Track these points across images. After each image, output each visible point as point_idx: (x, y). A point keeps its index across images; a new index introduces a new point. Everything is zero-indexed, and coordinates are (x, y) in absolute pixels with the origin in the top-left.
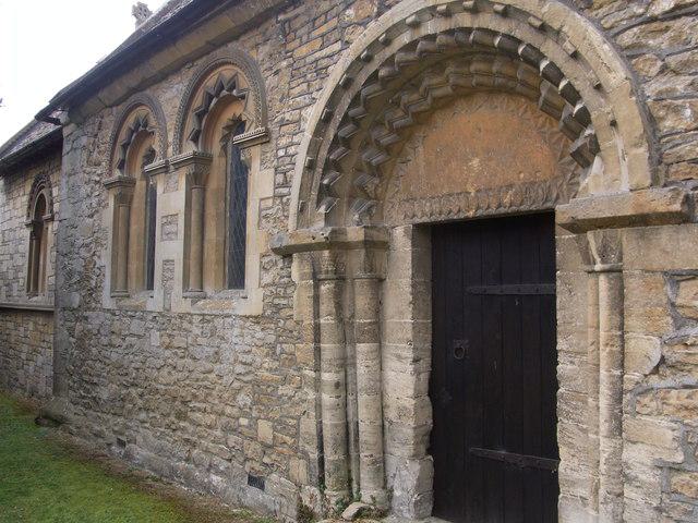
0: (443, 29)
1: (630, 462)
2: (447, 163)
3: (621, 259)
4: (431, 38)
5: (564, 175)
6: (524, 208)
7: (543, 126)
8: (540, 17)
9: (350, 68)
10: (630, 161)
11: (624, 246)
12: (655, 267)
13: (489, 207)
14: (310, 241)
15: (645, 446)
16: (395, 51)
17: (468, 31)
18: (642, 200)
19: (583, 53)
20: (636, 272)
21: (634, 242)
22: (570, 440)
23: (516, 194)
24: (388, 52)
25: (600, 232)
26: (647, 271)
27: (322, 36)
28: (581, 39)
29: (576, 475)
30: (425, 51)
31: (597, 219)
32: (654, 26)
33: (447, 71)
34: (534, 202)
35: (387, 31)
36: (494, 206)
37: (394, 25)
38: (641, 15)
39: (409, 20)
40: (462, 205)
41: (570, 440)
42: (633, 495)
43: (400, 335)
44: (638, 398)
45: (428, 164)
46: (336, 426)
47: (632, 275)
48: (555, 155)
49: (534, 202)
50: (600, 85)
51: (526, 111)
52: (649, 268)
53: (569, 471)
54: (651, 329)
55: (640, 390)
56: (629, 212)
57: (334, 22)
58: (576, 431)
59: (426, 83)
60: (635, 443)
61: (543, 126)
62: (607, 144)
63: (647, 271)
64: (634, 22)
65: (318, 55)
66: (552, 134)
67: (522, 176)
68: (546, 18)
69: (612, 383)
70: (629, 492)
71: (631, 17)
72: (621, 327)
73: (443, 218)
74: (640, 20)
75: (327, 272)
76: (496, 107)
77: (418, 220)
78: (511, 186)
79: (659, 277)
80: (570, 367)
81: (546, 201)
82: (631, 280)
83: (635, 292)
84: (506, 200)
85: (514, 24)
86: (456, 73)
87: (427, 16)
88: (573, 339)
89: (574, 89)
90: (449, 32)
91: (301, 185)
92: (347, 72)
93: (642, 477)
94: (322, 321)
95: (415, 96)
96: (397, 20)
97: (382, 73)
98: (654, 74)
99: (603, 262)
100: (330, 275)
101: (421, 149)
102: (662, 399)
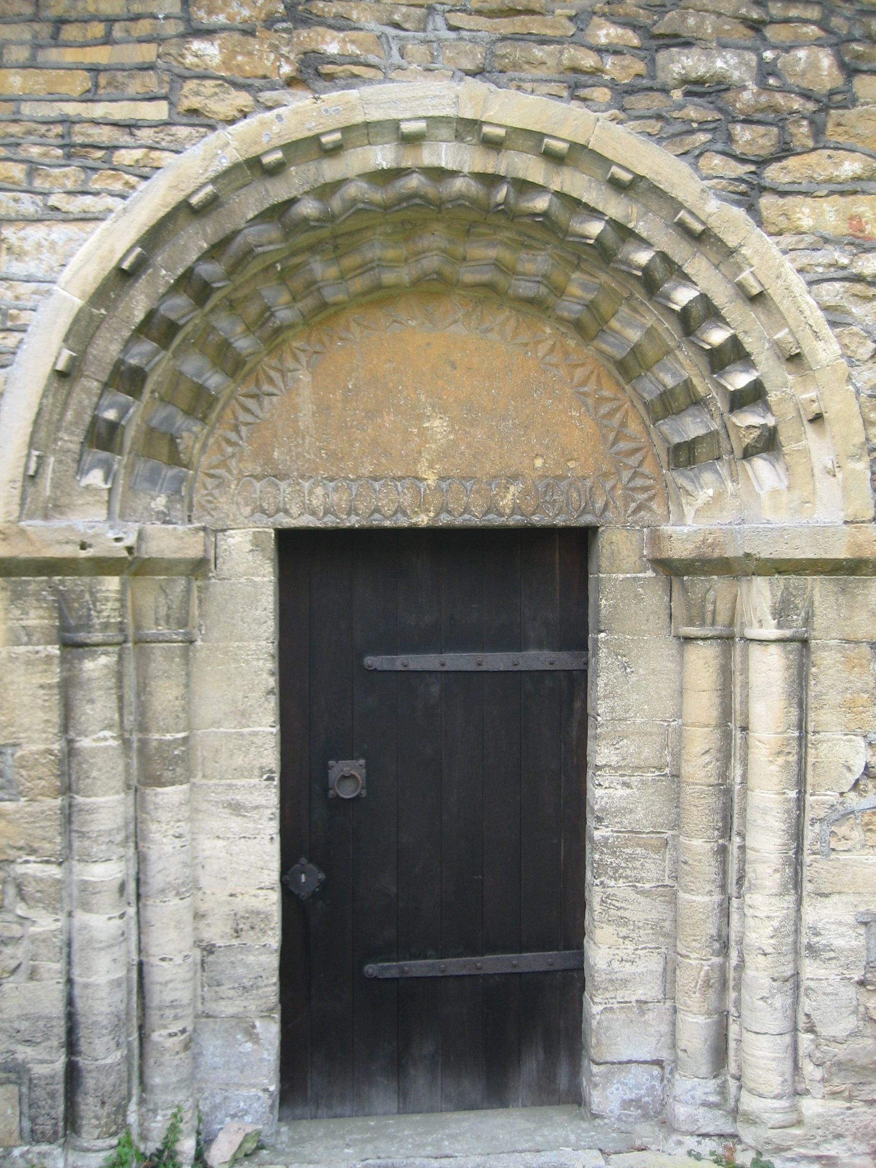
0: (478, 169)
1: (820, 925)
2: (372, 414)
3: (808, 621)
4: (439, 174)
5: (618, 473)
6: (537, 520)
7: (584, 383)
8: (703, 218)
9: (226, 173)
10: (845, 479)
11: (816, 604)
12: (860, 636)
13: (466, 510)
14: (71, 551)
15: (844, 898)
16: (351, 173)
17: (524, 187)
18: (861, 538)
19: (777, 299)
20: (833, 642)
21: (832, 598)
22: (619, 913)
23: (526, 492)
24: (331, 170)
25: (781, 580)
26: (848, 641)
27: (94, 70)
28: (773, 276)
29: (628, 968)
30: (421, 197)
31: (790, 560)
32: (859, 288)
33: (425, 242)
34: (560, 511)
35: (346, 130)
36: (477, 511)
37: (367, 124)
38: (844, 268)
39: (407, 127)
40: (407, 500)
41: (619, 913)
42: (822, 973)
43: (239, 760)
44: (833, 828)
45: (323, 409)
46: (117, 983)
47: (825, 647)
48: (604, 437)
49: (560, 511)
50: (798, 355)
51: (552, 350)
52: (852, 637)
53: (616, 965)
54: (853, 726)
55: (835, 816)
56: (841, 553)
57: (147, 53)
58: (633, 895)
59: (375, 252)
60: (826, 895)
61: (584, 383)
62: (794, 446)
63: (848, 641)
64: (832, 273)
65: (71, 109)
66: (601, 400)
67: (539, 462)
68: (713, 222)
69: (788, 811)
70: (810, 969)
71: (831, 265)
72: (801, 725)
73: (354, 521)
74: (844, 273)
75: (106, 626)
76: (491, 330)
77: (287, 522)
78: (514, 478)
79: (865, 649)
80: (622, 792)
81: (584, 512)
82: (825, 654)
83: (830, 672)
84: (507, 501)
85: (635, 210)
86: (444, 251)
87: (445, 132)
88: (629, 746)
89: (743, 349)
90: (490, 180)
91: (39, 414)
92: (214, 181)
93: (839, 943)
94: (85, 743)
95: (333, 271)
96: (375, 115)
97: (308, 208)
98: (866, 357)
99: (780, 626)
100: (113, 635)
101: (304, 376)
102: (867, 824)
